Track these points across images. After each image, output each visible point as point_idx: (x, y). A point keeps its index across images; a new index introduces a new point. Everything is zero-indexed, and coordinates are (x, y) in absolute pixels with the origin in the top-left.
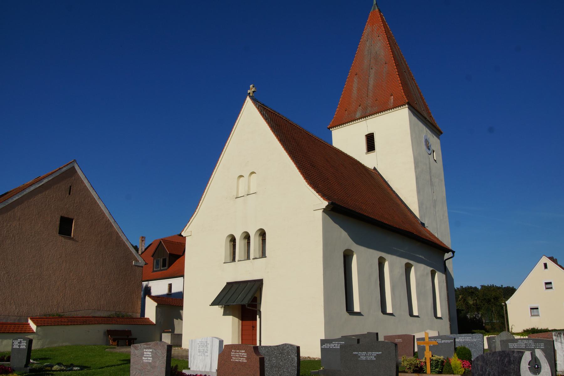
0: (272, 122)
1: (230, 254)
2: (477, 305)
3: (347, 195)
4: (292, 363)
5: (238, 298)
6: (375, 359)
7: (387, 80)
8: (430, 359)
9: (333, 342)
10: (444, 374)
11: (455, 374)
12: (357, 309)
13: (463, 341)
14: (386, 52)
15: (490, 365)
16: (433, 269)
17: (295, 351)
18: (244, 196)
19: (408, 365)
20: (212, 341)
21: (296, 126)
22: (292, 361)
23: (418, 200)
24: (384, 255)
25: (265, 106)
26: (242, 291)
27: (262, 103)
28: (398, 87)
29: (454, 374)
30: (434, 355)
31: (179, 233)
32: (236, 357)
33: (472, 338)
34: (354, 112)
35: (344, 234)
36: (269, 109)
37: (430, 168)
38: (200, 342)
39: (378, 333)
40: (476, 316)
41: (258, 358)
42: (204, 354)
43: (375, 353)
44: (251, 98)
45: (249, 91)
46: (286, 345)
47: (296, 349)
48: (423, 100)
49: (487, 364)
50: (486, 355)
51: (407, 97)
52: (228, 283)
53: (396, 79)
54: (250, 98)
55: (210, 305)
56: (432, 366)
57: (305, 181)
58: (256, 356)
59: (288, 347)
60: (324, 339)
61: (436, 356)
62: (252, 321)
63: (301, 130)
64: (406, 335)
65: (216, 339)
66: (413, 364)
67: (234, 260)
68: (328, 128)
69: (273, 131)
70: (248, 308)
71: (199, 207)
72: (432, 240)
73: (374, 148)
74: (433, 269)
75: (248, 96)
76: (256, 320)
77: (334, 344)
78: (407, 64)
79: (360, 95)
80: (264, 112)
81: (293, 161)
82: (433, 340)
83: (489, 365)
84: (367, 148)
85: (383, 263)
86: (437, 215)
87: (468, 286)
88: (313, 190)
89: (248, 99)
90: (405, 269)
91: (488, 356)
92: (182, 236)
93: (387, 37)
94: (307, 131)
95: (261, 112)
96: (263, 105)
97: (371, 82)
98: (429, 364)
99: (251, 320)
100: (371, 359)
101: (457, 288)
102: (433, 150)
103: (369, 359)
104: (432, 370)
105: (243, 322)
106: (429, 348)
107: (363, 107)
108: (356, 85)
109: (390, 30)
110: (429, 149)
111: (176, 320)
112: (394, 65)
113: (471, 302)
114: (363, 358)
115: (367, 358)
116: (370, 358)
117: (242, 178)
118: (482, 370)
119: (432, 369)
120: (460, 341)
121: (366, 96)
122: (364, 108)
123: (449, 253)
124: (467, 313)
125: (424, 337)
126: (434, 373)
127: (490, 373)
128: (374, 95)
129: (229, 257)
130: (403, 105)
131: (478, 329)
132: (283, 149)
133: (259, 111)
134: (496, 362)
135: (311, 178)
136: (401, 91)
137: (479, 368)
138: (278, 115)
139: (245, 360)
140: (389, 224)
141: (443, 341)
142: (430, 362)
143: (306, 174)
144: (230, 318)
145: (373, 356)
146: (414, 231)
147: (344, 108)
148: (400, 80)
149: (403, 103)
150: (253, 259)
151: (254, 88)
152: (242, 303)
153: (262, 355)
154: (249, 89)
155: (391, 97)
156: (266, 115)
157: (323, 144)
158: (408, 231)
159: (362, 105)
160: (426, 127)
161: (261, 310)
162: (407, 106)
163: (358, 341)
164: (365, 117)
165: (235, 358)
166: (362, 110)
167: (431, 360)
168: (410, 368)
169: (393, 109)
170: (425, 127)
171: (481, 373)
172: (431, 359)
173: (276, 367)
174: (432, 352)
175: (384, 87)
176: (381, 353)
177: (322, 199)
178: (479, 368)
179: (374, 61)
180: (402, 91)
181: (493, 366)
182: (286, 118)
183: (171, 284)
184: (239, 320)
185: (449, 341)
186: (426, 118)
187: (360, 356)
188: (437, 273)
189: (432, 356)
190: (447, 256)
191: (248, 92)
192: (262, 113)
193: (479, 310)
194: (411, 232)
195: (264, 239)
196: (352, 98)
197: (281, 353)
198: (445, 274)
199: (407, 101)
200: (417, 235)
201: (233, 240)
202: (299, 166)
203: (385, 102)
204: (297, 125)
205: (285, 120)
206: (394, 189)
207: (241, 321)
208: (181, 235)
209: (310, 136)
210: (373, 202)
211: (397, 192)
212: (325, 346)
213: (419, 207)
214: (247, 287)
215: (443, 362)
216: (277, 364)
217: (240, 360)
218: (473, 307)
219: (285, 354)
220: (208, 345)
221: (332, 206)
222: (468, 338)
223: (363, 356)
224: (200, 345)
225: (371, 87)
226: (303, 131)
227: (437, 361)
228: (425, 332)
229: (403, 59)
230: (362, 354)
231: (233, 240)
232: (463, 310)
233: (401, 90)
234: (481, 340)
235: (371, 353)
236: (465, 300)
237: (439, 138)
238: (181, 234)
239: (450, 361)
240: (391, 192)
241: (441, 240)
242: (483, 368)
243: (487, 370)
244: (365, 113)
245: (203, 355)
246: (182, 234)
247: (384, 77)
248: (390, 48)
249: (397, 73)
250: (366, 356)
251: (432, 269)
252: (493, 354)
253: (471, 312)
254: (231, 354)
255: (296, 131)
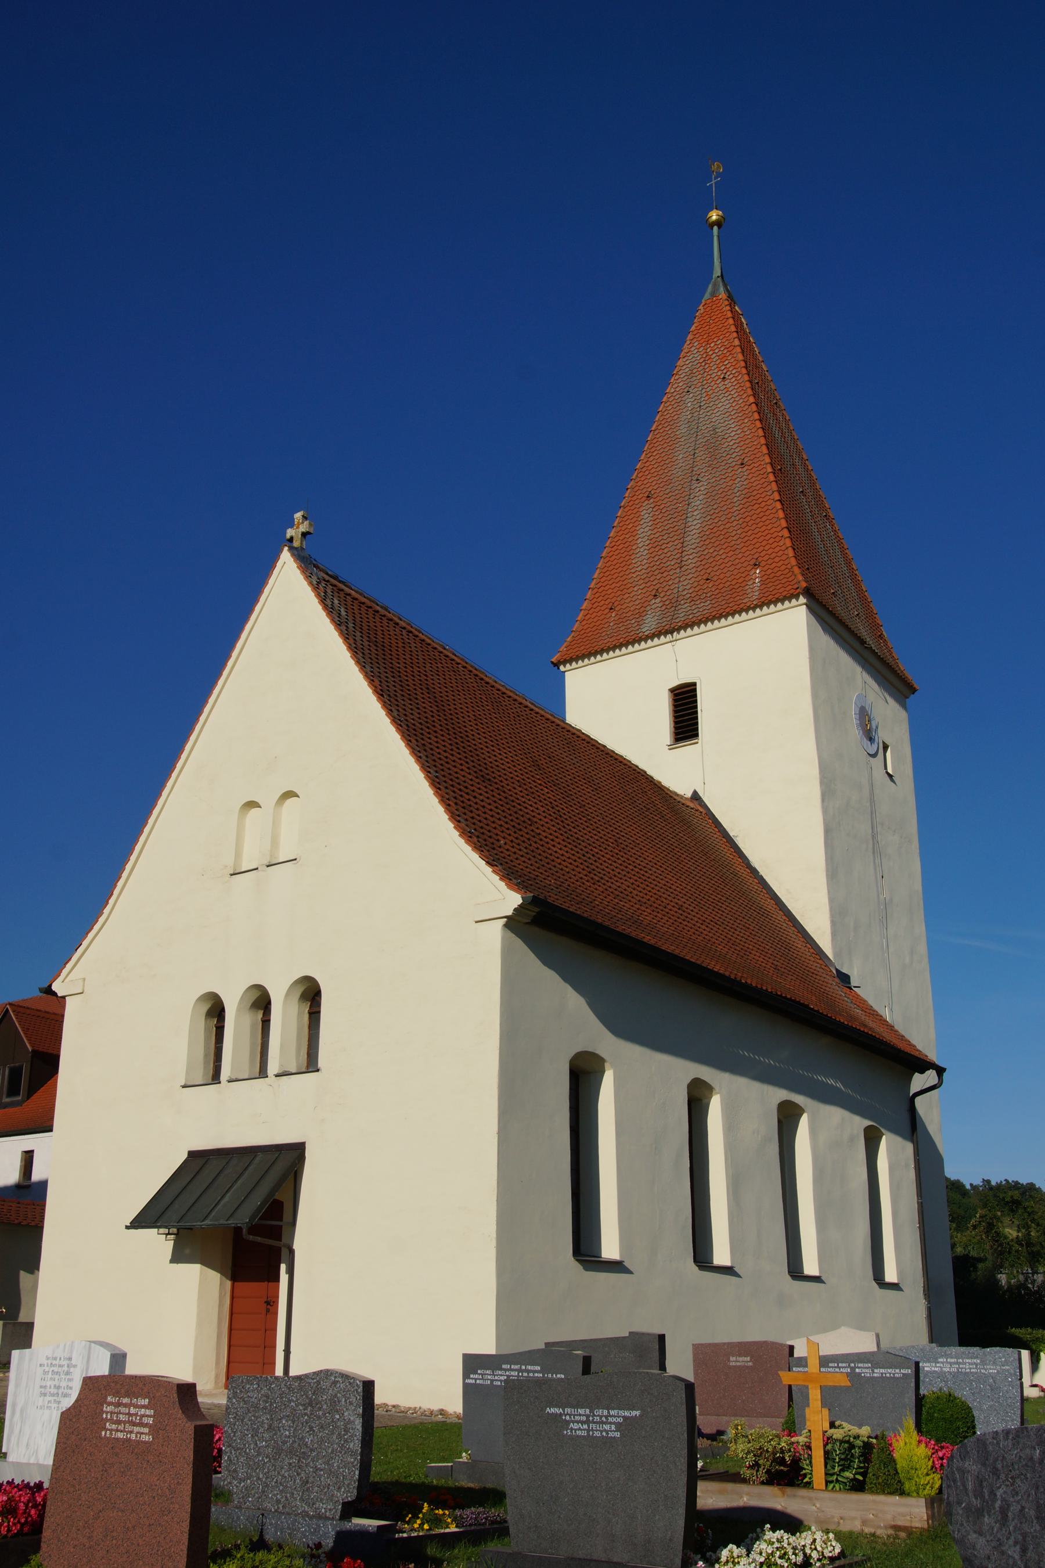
0: (358, 634)
1: (206, 1055)
2: (1029, 1244)
3: (592, 875)
4: (346, 1441)
5: (222, 1203)
6: (618, 1435)
7: (744, 516)
8: (824, 1435)
9: (504, 1366)
10: (872, 1492)
11: (909, 1495)
12: (610, 1249)
13: (954, 1370)
14: (746, 429)
15: (1007, 1476)
16: (870, 1123)
17: (357, 1398)
18: (257, 869)
19: (748, 1453)
20: (86, 1357)
21: (442, 650)
22: (346, 1431)
23: (831, 900)
24: (706, 1073)
25: (340, 582)
26: (236, 1181)
27: (330, 573)
28: (777, 539)
29: (902, 1493)
30: (837, 1423)
31: (46, 985)
32: (119, 1422)
33: (983, 1362)
34: (637, 616)
35: (574, 1002)
36: (353, 593)
37: (872, 800)
38: (48, 1358)
39: (664, 1336)
40: (1026, 1280)
41: (190, 1427)
42: (59, 1402)
43: (618, 1415)
44: (296, 553)
45: (290, 533)
46: (327, 1373)
47: (360, 1390)
48: (857, 583)
49: (995, 1472)
50: (993, 1438)
51: (806, 571)
52: (193, 1155)
53: (772, 516)
54: (293, 555)
55: (127, 1227)
56: (830, 1463)
57: (451, 825)
58: (185, 1420)
59: (335, 1383)
60: (493, 1352)
61: (845, 1424)
62: (266, 1283)
63: (458, 664)
64: (765, 1342)
65: (102, 1349)
66: (767, 1451)
67: (216, 1078)
68: (552, 662)
69: (358, 662)
70: (251, 1238)
71: (111, 901)
72: (871, 1029)
73: (697, 729)
74: (870, 1123)
75: (286, 548)
76: (277, 1279)
77: (506, 1370)
78: (810, 468)
79: (658, 563)
80: (336, 602)
81: (418, 758)
82: (844, 1365)
83: (1003, 1476)
84: (673, 729)
85: (705, 1101)
86: (891, 950)
87: (1006, 1180)
88: (475, 856)
89: (286, 556)
90: (780, 1122)
91: (998, 1443)
92: (55, 994)
93: (750, 381)
94: (476, 669)
95: (323, 600)
96: (335, 578)
97: (695, 523)
98: (822, 1453)
99: (263, 1281)
100: (604, 1434)
101: (971, 1185)
102: (884, 743)
103: (597, 1434)
104: (832, 1475)
105: (236, 1283)
106: (819, 1397)
107: (665, 599)
108: (646, 530)
109: (770, 378)
110: (871, 739)
111: (28, 1275)
112: (770, 469)
113: (1011, 1233)
114: (578, 1429)
115: (592, 1430)
116: (601, 1432)
117: (254, 811)
118: (979, 1494)
119: (832, 1471)
120: (942, 1371)
121: (677, 566)
122: (667, 603)
123: (928, 1072)
124: (999, 1267)
125: (806, 1355)
126: (837, 1486)
127: (1009, 1506)
128: (703, 563)
129: (202, 1066)
130: (789, 598)
131: (1026, 1327)
132: (387, 721)
133: (318, 595)
134: (1026, 1465)
135: (473, 818)
136: (786, 552)
137: (970, 1486)
138: (383, 612)
139: (148, 1434)
140: (727, 974)
141: (878, 1372)
142: (825, 1446)
143: (456, 804)
144: (193, 1272)
145: (611, 1423)
146: (814, 998)
147: (606, 603)
148: (786, 518)
149: (792, 591)
150: (277, 1076)
151: (306, 523)
152: (232, 1222)
153: (208, 1420)
154: (291, 525)
155: (753, 571)
156: (342, 610)
157: (528, 712)
158: (790, 999)
159: (662, 595)
160: (863, 667)
161: (295, 1247)
162: (802, 600)
163: (587, 1362)
164: (672, 633)
165: (114, 1427)
166: (664, 608)
167: (828, 1440)
168: (756, 1465)
169: (758, 610)
170: (859, 669)
171: (976, 1503)
172: (828, 1434)
173: (291, 1452)
174: (829, 1410)
175: (734, 538)
176: (638, 1413)
177: (502, 885)
178: (970, 1486)
179: (705, 456)
180: (791, 552)
181: (1018, 1481)
182: (409, 624)
183: (32, 1151)
184: (224, 1278)
185: (898, 1373)
186: (863, 642)
187: (568, 1422)
188: (884, 1137)
189: (832, 1425)
190: (919, 1081)
191: (288, 536)
192: (329, 602)
193: (1038, 1261)
194: (799, 1003)
195: (315, 1010)
196: (633, 571)
197: (310, 1404)
198: (912, 1141)
199: (804, 584)
200: (818, 1011)
201: (216, 1010)
202: (437, 777)
203: (736, 587)
204: (445, 649)
205: (404, 628)
206: (756, 860)
207: (228, 1284)
208: (49, 991)
209: (487, 683)
210: (680, 903)
211: (762, 872)
212: (484, 1378)
213: (833, 923)
214: (251, 1168)
215: (867, 1447)
216: (294, 1442)
217: (131, 1432)
218: (1017, 1251)
219: (325, 1407)
220: (72, 1370)
221: (537, 910)
222: (970, 1361)
223: (578, 1422)
224: (47, 1369)
225: (692, 539)
226: (465, 667)
227: (848, 1444)
228: (808, 1339)
229: (799, 453)
230: (574, 1415)
231: (216, 1010)
232: (980, 1260)
233: (787, 548)
234: (1012, 1372)
235: (605, 1412)
236: (990, 1226)
237: (904, 706)
238: (50, 986)
239: (891, 1445)
240: (744, 872)
241: (903, 1033)
242: (985, 1484)
243: (998, 1494)
244: (670, 617)
245: (56, 1405)
246: (54, 987)
247: (735, 509)
248: (756, 416)
249: (777, 496)
250: (587, 1422)
251: (868, 1123)
252: (1018, 1436)
253: (1012, 1266)
254: (103, 1412)
255: (439, 665)
